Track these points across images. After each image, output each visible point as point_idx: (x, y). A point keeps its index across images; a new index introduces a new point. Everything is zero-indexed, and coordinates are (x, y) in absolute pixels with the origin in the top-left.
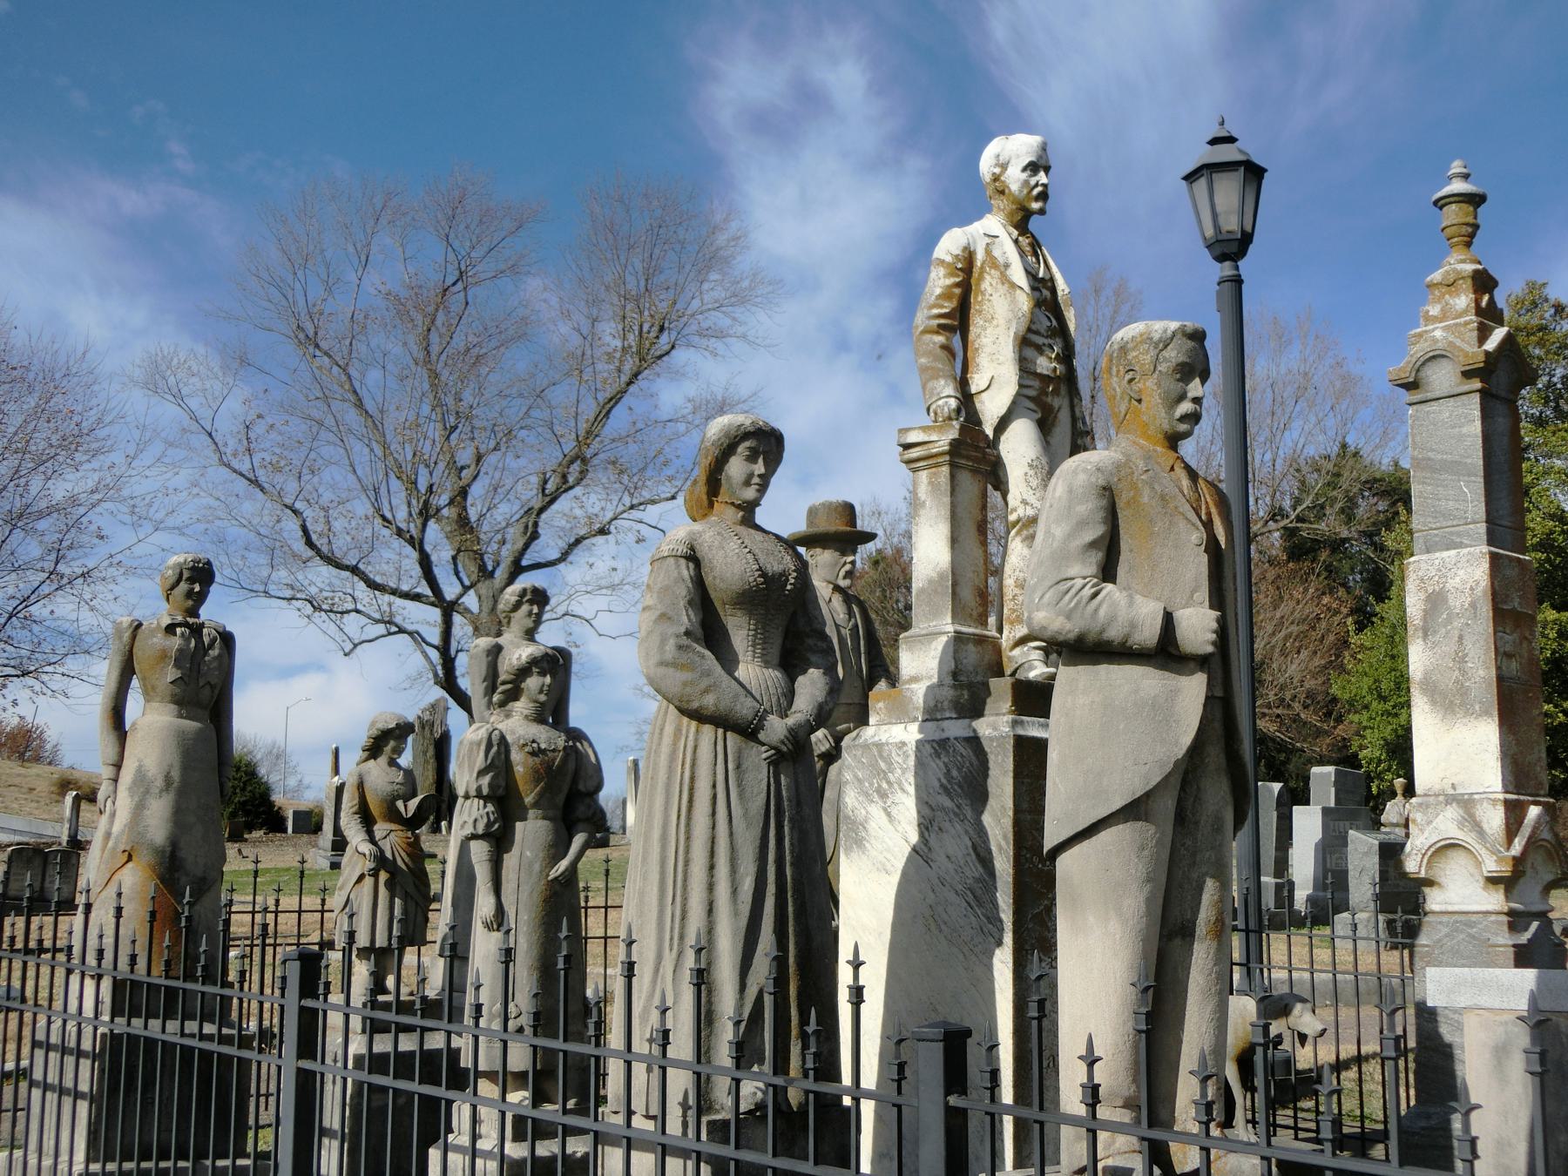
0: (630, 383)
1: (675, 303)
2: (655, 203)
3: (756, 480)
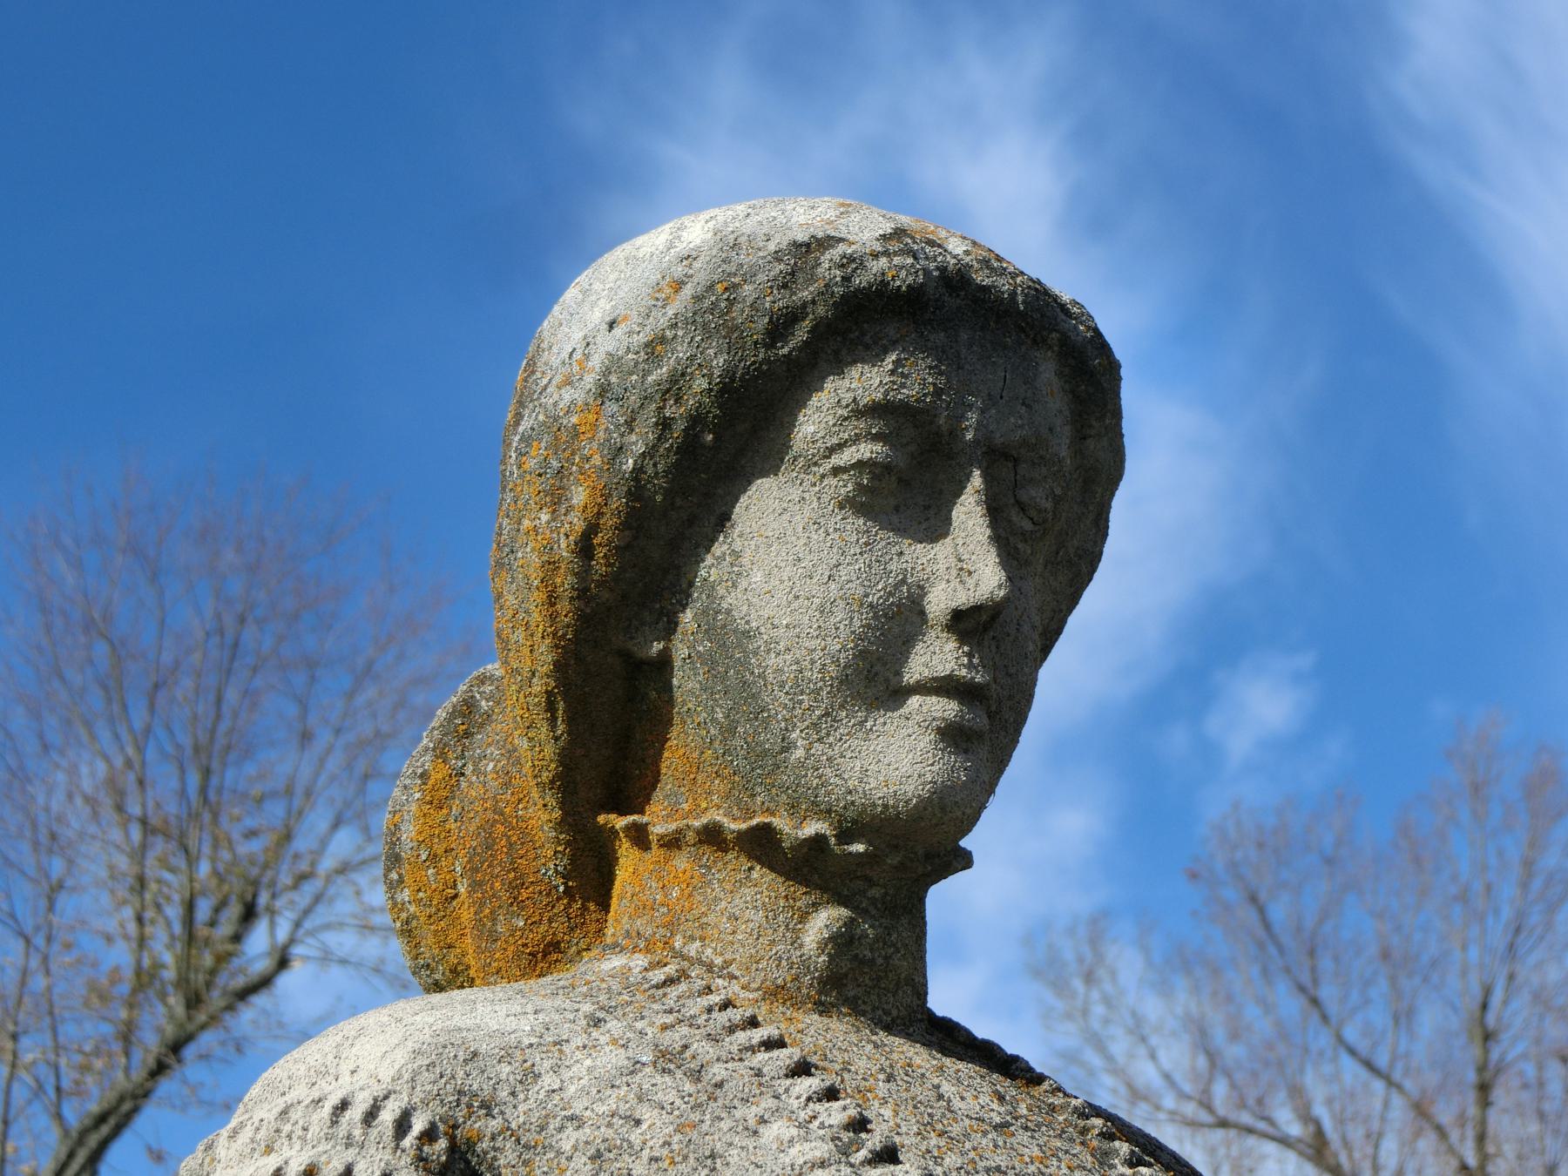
0: (160, 1069)
1: (288, 837)
2: (229, 556)
3: (937, 655)
